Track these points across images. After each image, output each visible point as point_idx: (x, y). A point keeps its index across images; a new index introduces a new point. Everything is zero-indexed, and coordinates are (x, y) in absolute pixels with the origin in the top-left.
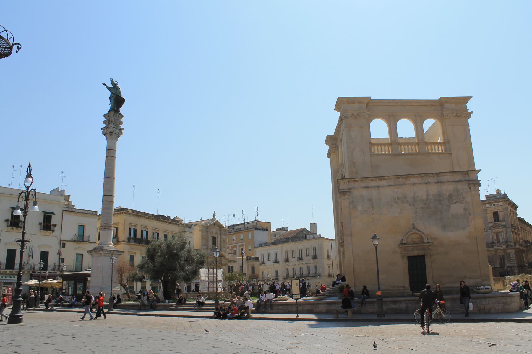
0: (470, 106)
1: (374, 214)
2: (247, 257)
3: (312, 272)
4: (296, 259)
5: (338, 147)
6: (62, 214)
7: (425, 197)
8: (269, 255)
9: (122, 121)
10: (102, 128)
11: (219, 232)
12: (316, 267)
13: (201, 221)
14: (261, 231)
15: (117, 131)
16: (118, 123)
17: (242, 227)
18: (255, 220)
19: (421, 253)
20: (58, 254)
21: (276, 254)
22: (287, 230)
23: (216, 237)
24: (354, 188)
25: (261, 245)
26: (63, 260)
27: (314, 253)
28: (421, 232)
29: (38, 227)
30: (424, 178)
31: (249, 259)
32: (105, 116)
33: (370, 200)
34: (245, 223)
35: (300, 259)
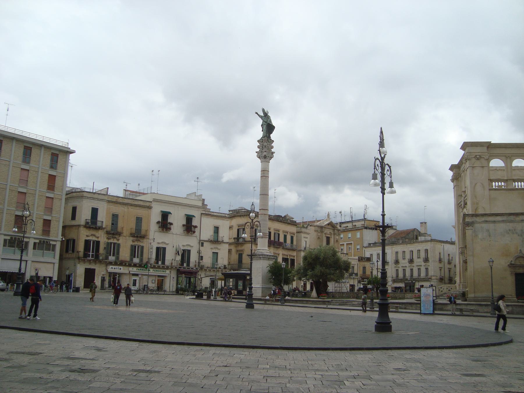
1: (490, 241)
2: (359, 257)
4: (406, 261)
9: (273, 146)
10: (256, 152)
11: (332, 233)
14: (370, 230)
18: (363, 218)
20: (198, 252)
23: (329, 237)
26: (202, 257)
27: (425, 254)
31: (360, 259)
32: (258, 141)
33: (488, 231)
34: (352, 221)
35: (411, 261)
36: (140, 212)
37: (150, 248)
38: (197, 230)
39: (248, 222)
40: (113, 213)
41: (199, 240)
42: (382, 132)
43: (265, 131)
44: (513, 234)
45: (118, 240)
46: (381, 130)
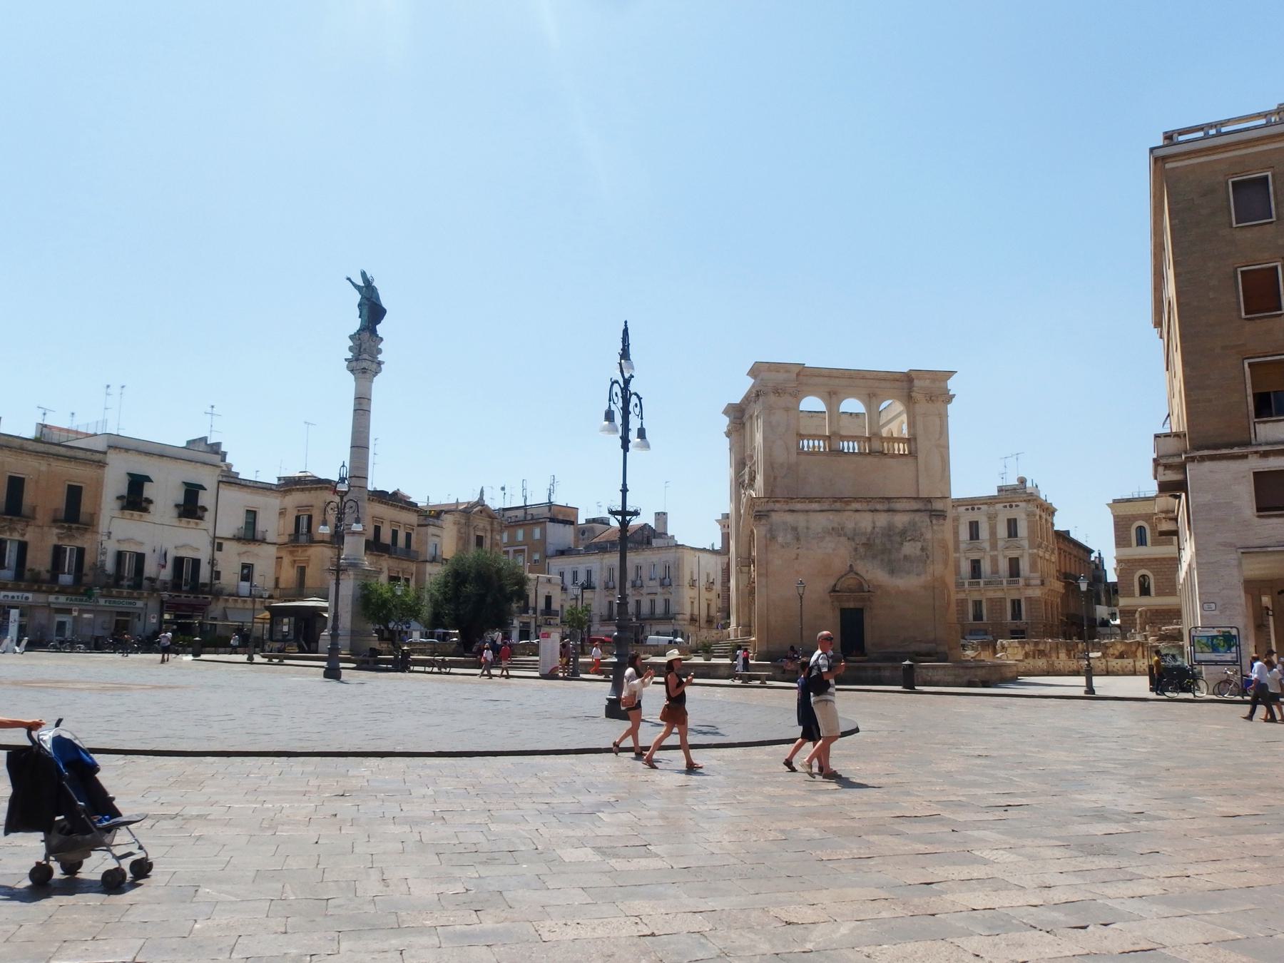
0: (952, 385)
3: (659, 609)
5: (744, 424)
6: (216, 491)
7: (869, 529)
8: (575, 574)
10: (346, 360)
11: (488, 528)
12: (667, 602)
13: (457, 503)
15: (375, 366)
16: (375, 352)
17: (520, 513)
19: (859, 605)
20: (209, 563)
21: (589, 573)
22: (607, 522)
23: (482, 536)
24: (773, 511)
25: (561, 553)
26: (218, 573)
28: (861, 576)
29: (174, 512)
30: (870, 504)
32: (351, 337)
33: (795, 529)
34: (526, 506)
36: (78, 474)
37: (100, 551)
38: (209, 516)
39: (332, 502)
40: (11, 474)
41: (213, 536)
42: (626, 332)
43: (366, 318)
44: (840, 536)
45: (23, 535)
46: (626, 326)
